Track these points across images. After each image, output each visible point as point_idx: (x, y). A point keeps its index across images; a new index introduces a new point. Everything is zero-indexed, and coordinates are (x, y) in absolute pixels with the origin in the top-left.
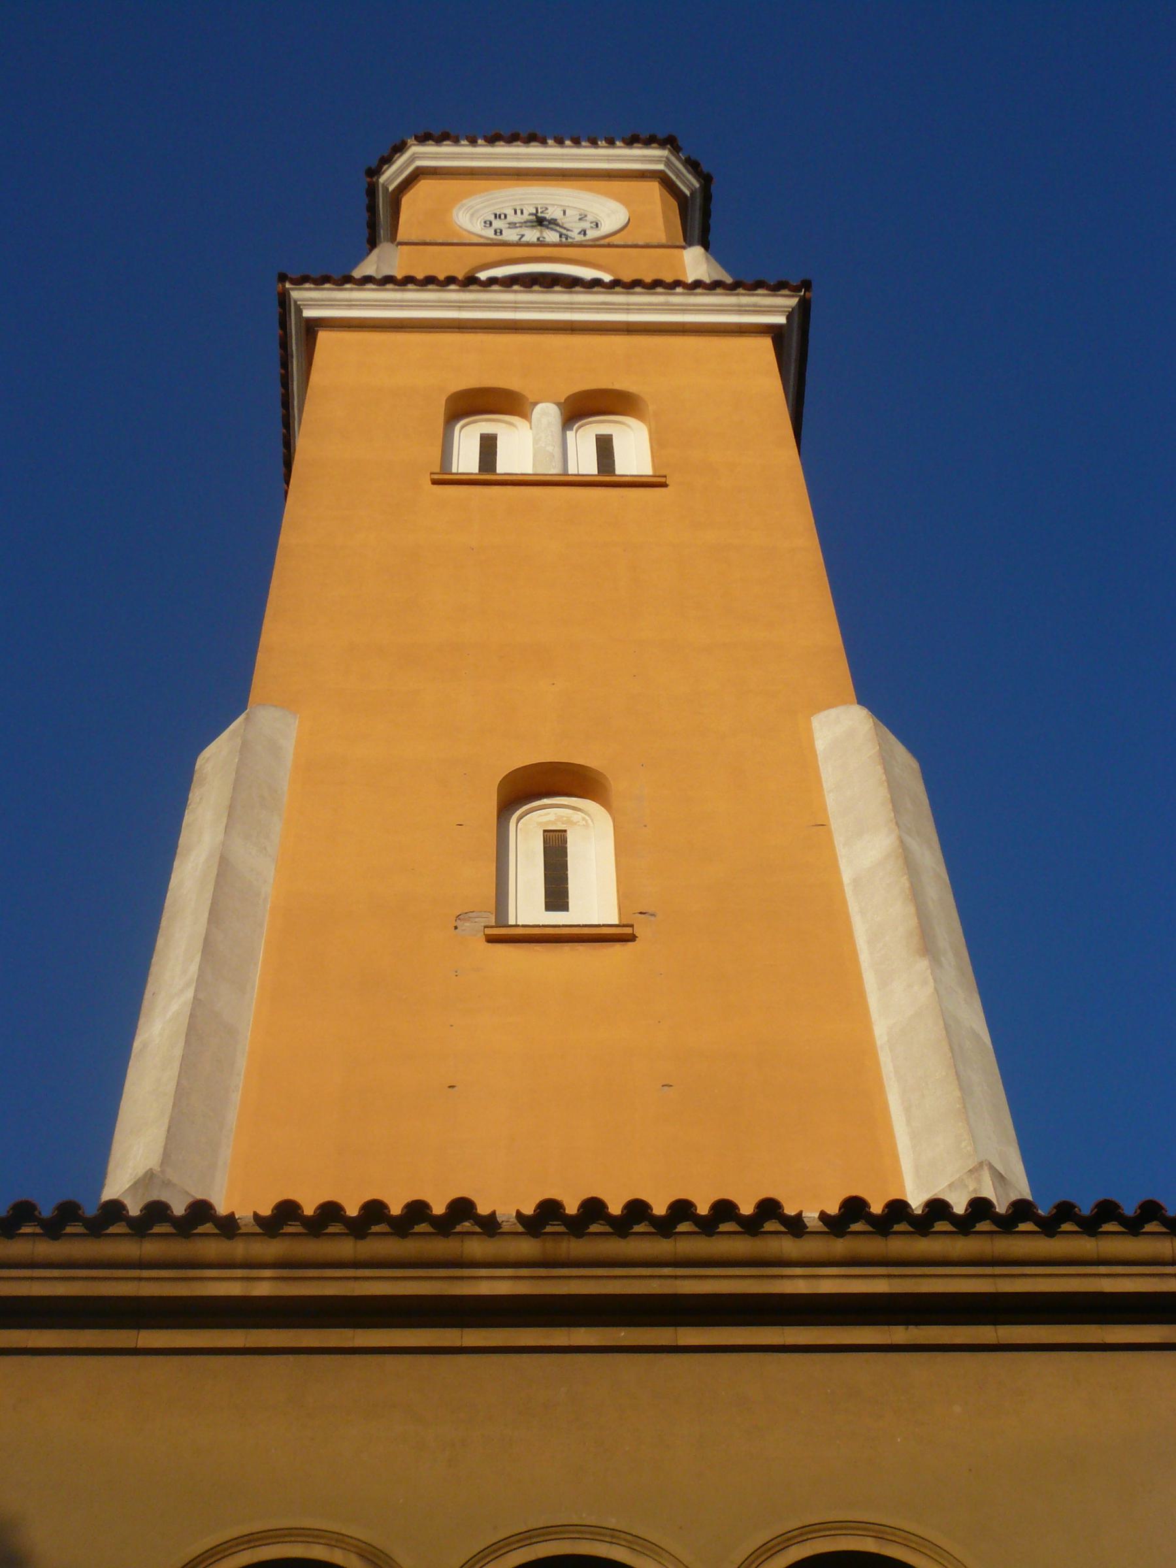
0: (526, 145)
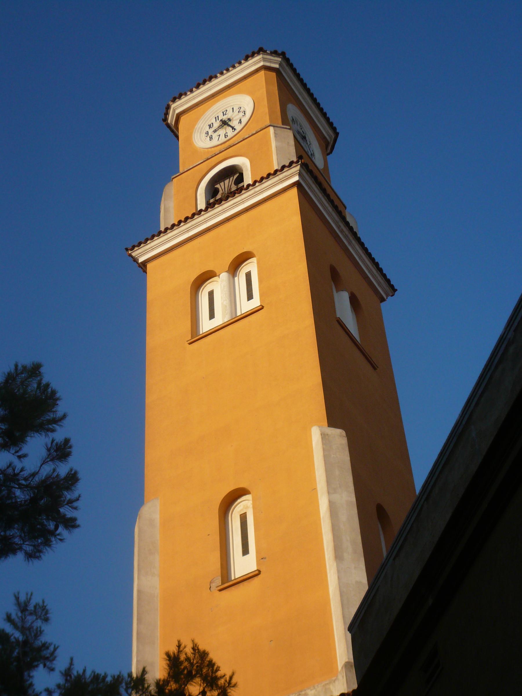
0: (211, 82)
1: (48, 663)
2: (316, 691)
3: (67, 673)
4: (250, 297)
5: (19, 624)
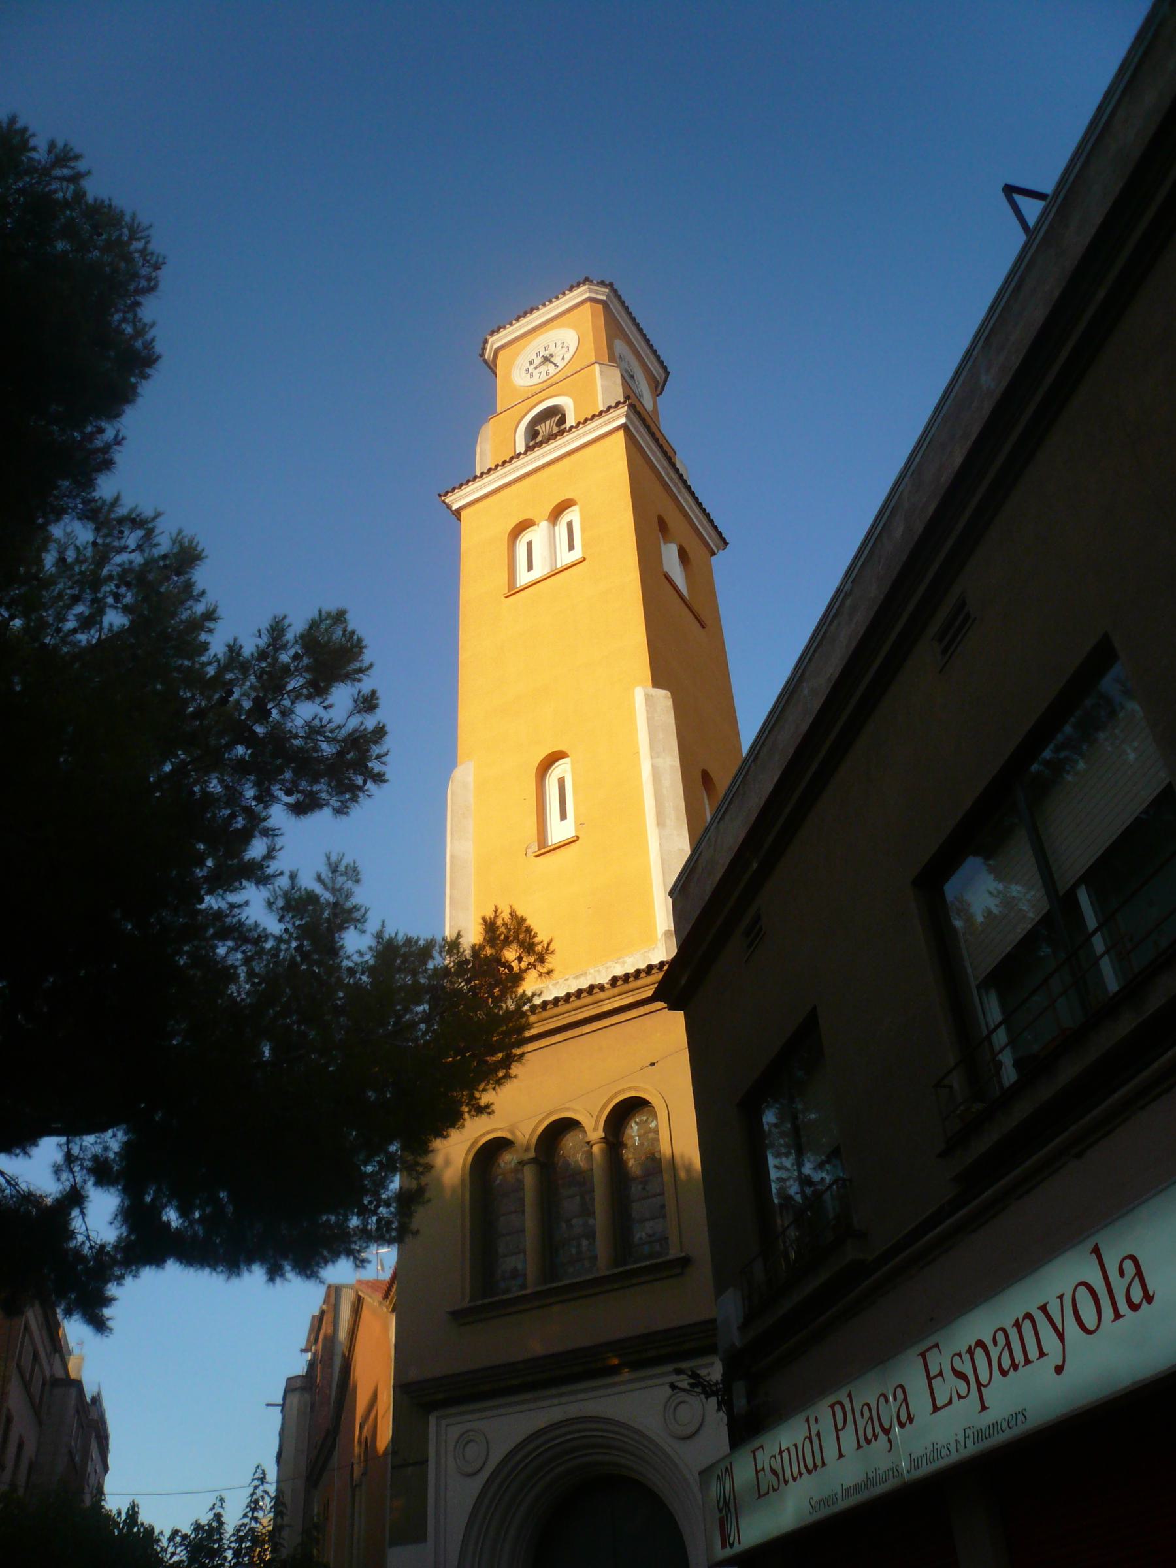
1: (359, 925)
2: (634, 958)
3: (379, 936)
4: (571, 547)
5: (330, 885)
